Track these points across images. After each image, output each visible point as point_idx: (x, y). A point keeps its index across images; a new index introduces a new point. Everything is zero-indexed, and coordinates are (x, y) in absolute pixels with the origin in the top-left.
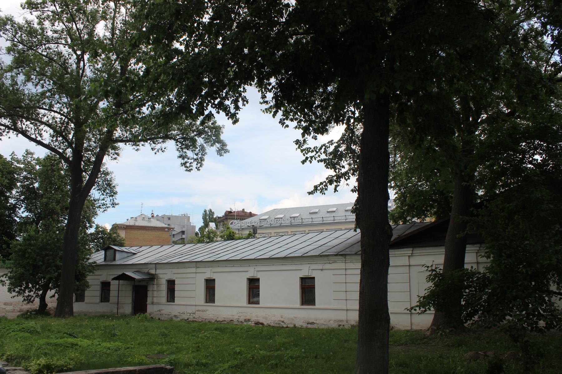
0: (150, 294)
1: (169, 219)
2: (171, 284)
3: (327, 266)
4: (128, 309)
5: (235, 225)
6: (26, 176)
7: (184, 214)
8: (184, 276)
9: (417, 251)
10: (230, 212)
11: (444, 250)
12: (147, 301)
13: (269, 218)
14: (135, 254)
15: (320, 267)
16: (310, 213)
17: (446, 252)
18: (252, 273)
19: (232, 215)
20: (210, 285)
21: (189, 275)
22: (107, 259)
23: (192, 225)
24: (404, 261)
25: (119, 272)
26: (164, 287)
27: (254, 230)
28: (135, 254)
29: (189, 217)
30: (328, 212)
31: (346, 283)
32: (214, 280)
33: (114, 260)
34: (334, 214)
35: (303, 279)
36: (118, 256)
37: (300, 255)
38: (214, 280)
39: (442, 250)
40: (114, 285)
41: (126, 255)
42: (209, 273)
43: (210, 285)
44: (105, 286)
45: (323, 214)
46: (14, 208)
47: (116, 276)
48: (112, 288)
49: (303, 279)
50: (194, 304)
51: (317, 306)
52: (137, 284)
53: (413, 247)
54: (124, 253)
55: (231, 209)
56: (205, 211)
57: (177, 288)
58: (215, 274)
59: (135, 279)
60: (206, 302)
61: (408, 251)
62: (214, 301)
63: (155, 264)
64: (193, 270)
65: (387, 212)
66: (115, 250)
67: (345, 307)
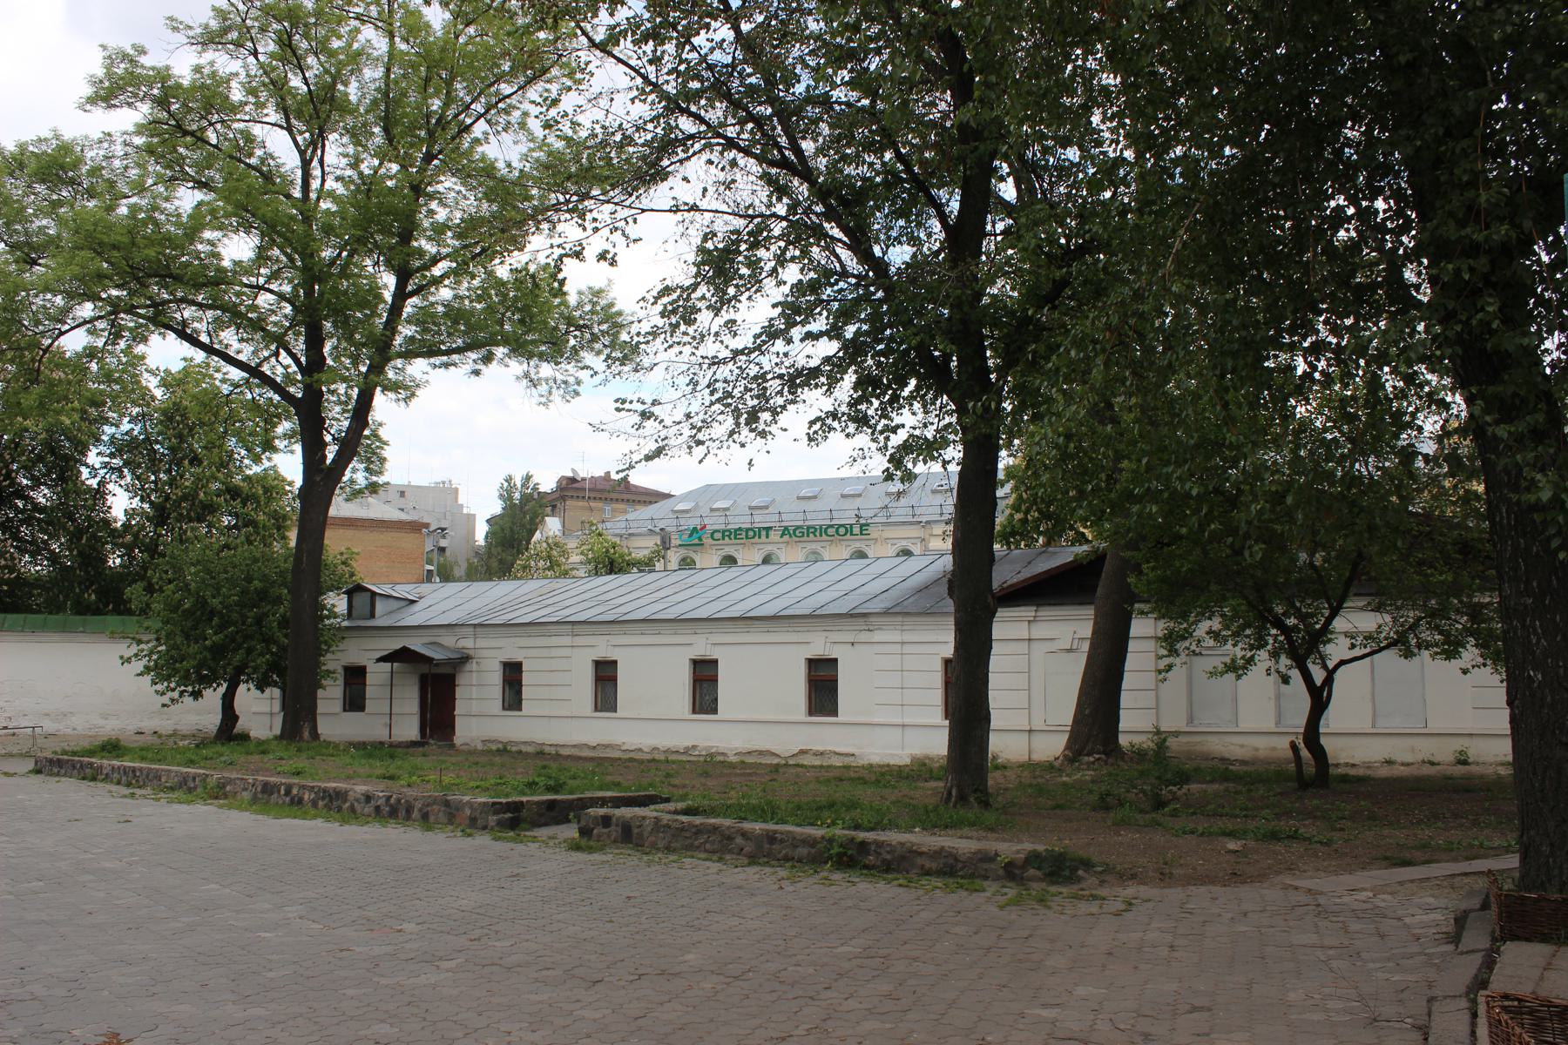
0: (459, 692)
1: (402, 494)
2: (513, 674)
3: (864, 636)
4: (408, 728)
5: (618, 524)
6: (253, 461)
7: (444, 483)
8: (545, 653)
9: (1046, 612)
10: (573, 480)
11: (1092, 612)
12: (454, 709)
13: (696, 507)
14: (413, 602)
15: (850, 637)
16: (798, 498)
17: (1096, 616)
18: (702, 647)
19: (578, 489)
20: (605, 674)
21: (555, 652)
22: (355, 613)
23: (465, 511)
24: (1021, 631)
25: (395, 644)
26: (496, 678)
27: (664, 542)
28: (413, 602)
29: (456, 490)
30: (843, 496)
31: (1030, 731)
32: (615, 662)
33: (372, 615)
34: (858, 502)
35: (813, 664)
36: (380, 607)
37: (807, 612)
38: (615, 662)
39: (1089, 612)
40: (377, 674)
41: (396, 604)
42: (603, 648)
43: (605, 674)
44: (355, 675)
45: (830, 501)
46: (100, 493)
47: (386, 653)
48: (370, 679)
49: (813, 664)
50: (569, 714)
51: (841, 718)
52: (435, 670)
53: (1038, 605)
54: (391, 601)
55: (573, 470)
56: (509, 479)
57: (526, 679)
58: (617, 649)
59: (433, 659)
60: (694, 712)
61: (1027, 612)
62: (351, 710)
63: (475, 626)
64: (567, 640)
65: (962, 189)
66: (374, 594)
67: (899, 721)
